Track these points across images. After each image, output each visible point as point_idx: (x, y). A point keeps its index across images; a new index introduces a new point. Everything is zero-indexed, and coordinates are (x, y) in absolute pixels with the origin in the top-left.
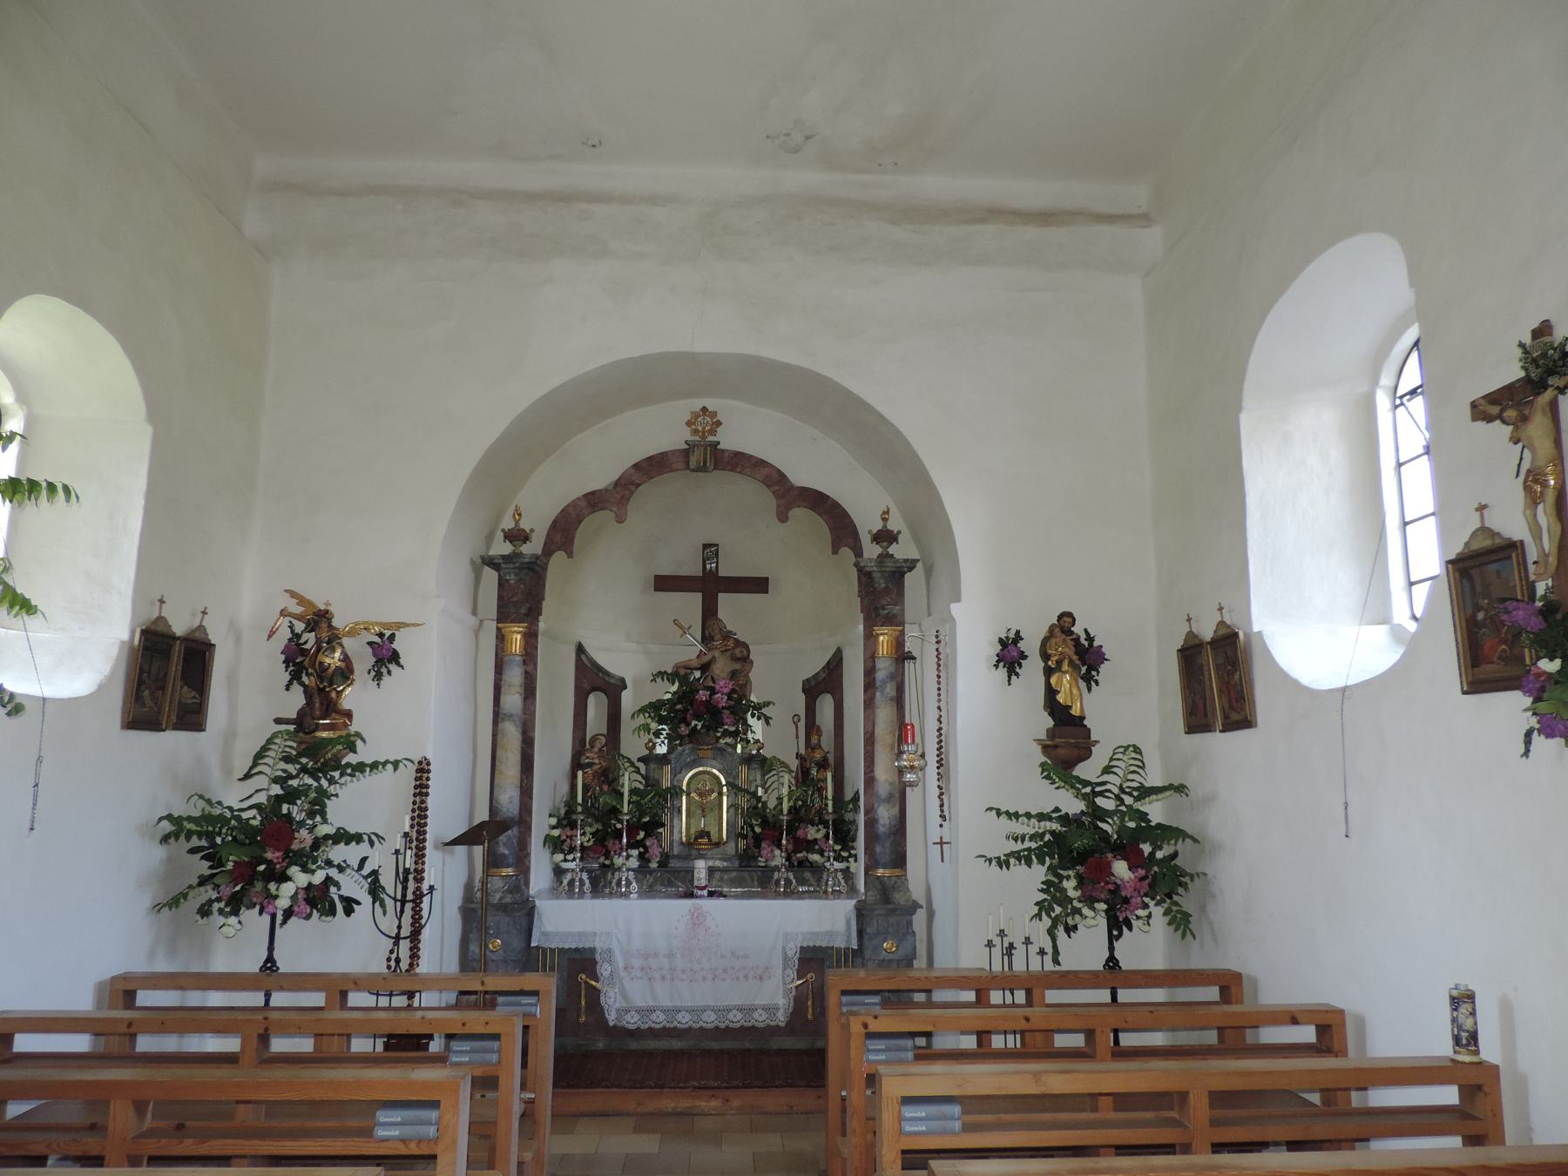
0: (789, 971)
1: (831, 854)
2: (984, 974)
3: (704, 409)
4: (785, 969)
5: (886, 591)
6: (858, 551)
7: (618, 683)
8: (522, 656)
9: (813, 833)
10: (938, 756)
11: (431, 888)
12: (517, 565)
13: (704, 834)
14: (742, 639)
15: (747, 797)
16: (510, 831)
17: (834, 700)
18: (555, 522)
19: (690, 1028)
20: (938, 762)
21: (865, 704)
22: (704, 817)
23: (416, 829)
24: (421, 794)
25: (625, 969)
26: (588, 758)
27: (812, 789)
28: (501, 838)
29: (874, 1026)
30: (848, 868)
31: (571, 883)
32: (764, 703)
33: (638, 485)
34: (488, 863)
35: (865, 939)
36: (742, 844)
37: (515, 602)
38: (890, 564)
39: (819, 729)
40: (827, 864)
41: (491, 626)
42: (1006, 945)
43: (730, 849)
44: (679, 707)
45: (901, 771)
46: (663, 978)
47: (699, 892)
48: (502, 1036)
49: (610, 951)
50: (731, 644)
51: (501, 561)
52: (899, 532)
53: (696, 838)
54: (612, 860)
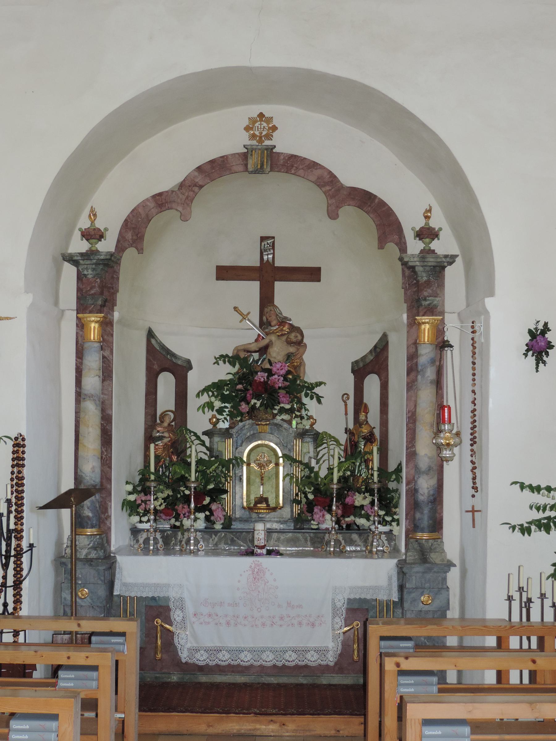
0: (337, 620)
1: (376, 519)
2: (504, 624)
3: (261, 115)
4: (334, 617)
5: (428, 283)
6: (403, 248)
7: (185, 365)
8: (100, 342)
9: (359, 500)
10: (472, 434)
11: (31, 546)
12: (95, 261)
13: (262, 500)
14: (296, 324)
15: (302, 467)
16: (93, 497)
17: (381, 380)
18: (126, 221)
19: (252, 666)
20: (471, 440)
21: (407, 385)
22: (262, 485)
23: (14, 495)
24: (18, 465)
25: (195, 615)
26: (158, 431)
27: (359, 461)
28: (85, 502)
29: (406, 665)
30: (391, 531)
31: (147, 541)
32: (316, 383)
33: (201, 187)
34: (75, 525)
35: (405, 593)
36: (296, 509)
37: (92, 294)
38: (432, 260)
39: (366, 406)
40: (373, 528)
41: (71, 317)
42: (524, 599)
43: (286, 513)
44: (240, 387)
45: (439, 447)
46: (228, 623)
47: (259, 551)
48: (100, 669)
49: (182, 600)
50: (286, 328)
51: (79, 258)
52: (440, 229)
53: (256, 504)
54: (181, 522)
